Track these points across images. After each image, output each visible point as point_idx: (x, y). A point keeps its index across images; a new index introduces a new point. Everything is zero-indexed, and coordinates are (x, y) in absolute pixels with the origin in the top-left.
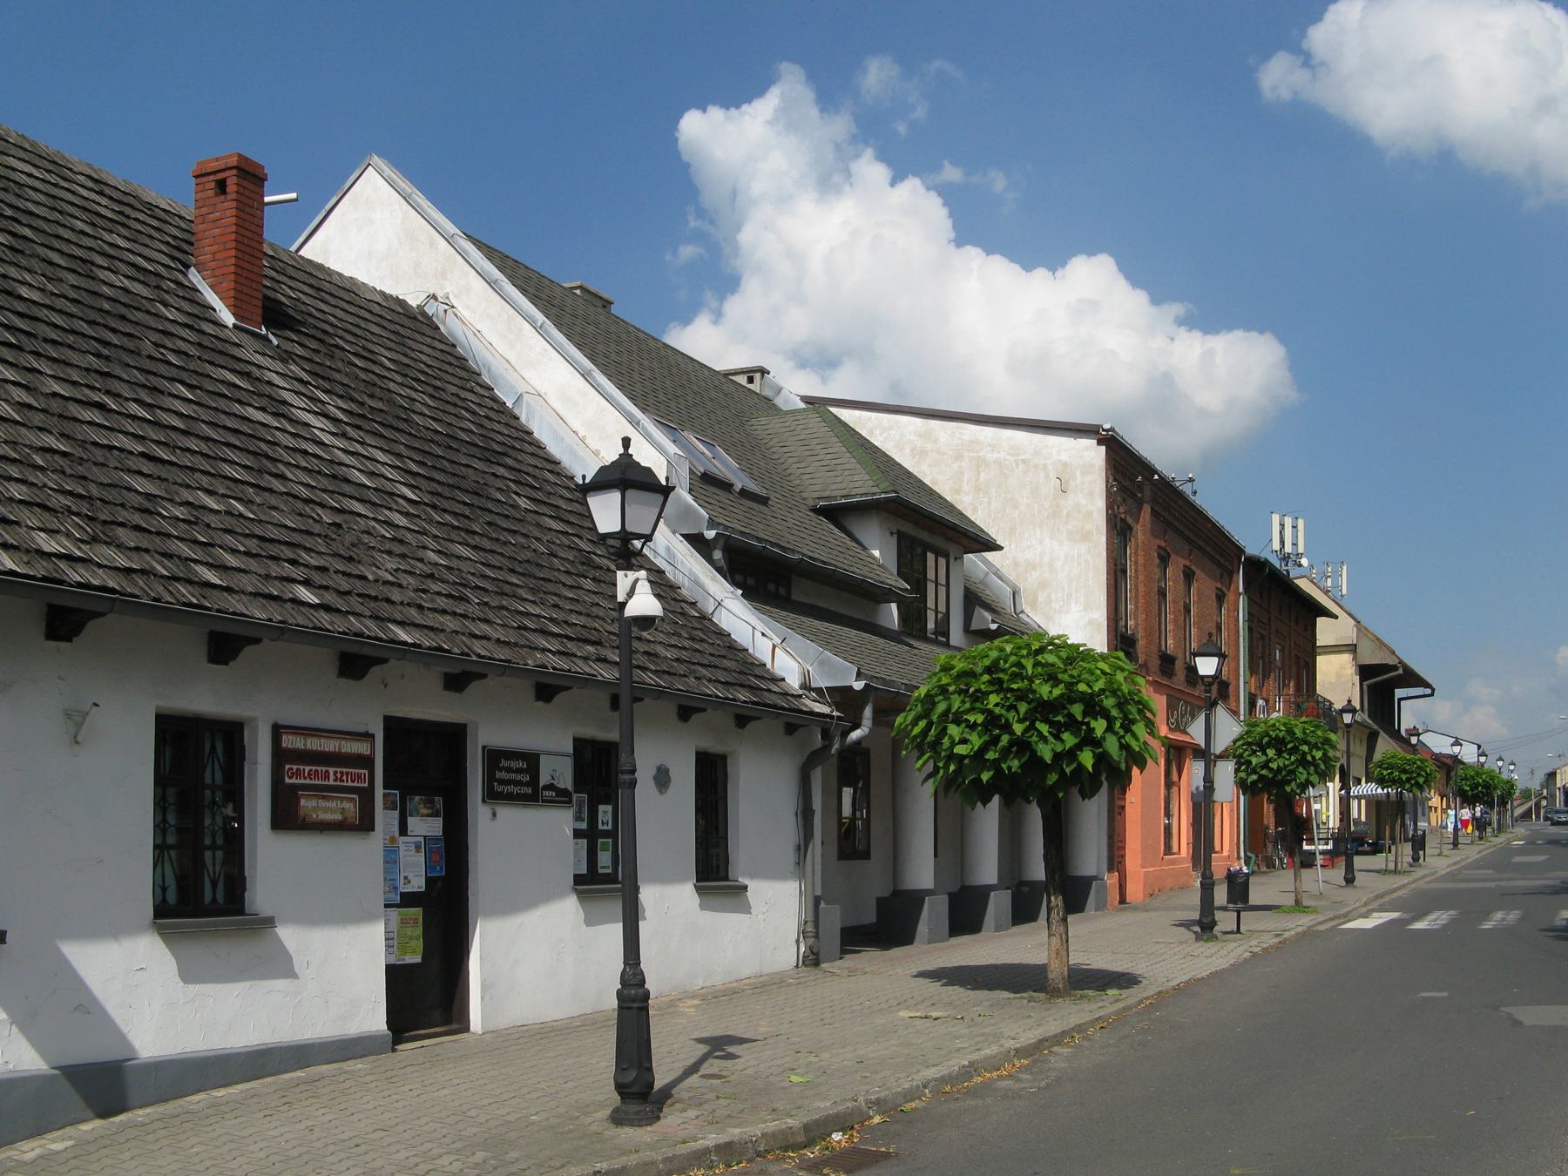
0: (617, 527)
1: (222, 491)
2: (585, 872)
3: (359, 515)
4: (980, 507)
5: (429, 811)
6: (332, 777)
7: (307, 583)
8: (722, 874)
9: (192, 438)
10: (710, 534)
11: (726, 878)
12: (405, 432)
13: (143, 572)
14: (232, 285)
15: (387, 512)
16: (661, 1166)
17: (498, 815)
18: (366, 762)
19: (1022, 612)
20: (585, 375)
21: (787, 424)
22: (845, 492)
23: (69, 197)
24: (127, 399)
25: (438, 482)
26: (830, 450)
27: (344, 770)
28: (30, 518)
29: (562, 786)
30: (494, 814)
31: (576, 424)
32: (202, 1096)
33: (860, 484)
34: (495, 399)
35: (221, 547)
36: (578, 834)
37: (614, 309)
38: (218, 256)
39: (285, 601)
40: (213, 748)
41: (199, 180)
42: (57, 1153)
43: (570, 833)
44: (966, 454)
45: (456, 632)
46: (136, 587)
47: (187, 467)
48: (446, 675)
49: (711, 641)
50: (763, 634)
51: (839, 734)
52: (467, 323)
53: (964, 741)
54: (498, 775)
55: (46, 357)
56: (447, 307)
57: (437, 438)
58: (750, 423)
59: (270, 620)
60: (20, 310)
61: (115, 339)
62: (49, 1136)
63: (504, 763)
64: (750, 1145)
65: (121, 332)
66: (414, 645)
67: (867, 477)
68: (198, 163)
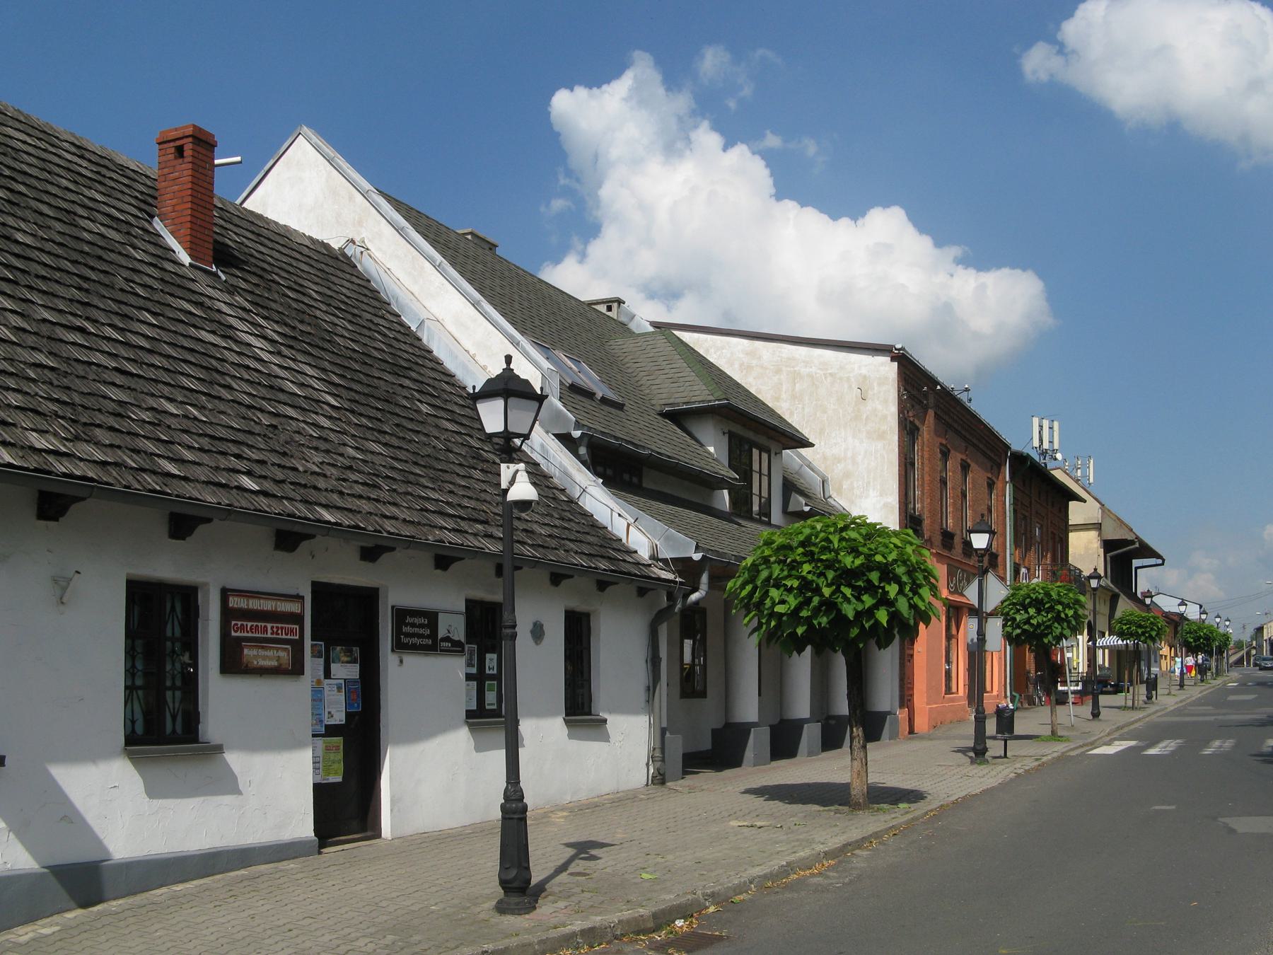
0: (501, 428)
1: (180, 399)
2: (475, 708)
3: (292, 418)
4: (796, 412)
5: (349, 659)
6: (269, 631)
7: (249, 473)
8: (586, 710)
9: (156, 356)
10: (577, 434)
11: (590, 713)
12: (329, 351)
13: (116, 464)
14: (189, 231)
15: (314, 416)
16: (536, 947)
17: (404, 661)
18: (297, 619)
19: (830, 497)
20: (475, 305)
21: (639, 344)
22: (686, 400)
23: (56, 160)
24: (103, 324)
25: (356, 392)
26: (674, 366)
27: (280, 625)
28: (25, 421)
29: (456, 638)
30: (401, 661)
31: (467, 344)
32: (164, 890)
33: (698, 393)
34: (402, 324)
35: (179, 444)
36: (469, 677)
37: (499, 251)
38: (177, 208)
39: (232, 488)
40: (173, 608)
41: (162, 146)
42: (46, 936)
43: (463, 677)
44: (784, 369)
45: (371, 513)
46: (110, 477)
47: (152, 379)
48: (362, 548)
49: (577, 521)
50: (619, 515)
51: (681, 596)
52: (379, 262)
53: (783, 602)
54: (405, 629)
55: (38, 290)
56: (363, 250)
57: (355, 356)
58: (609, 344)
59: (219, 504)
60: (16, 251)
61: (93, 276)
62: (40, 922)
63: (409, 620)
64: (609, 930)
65: (99, 270)
66: (336, 524)
67: (704, 387)
68: (161, 133)
